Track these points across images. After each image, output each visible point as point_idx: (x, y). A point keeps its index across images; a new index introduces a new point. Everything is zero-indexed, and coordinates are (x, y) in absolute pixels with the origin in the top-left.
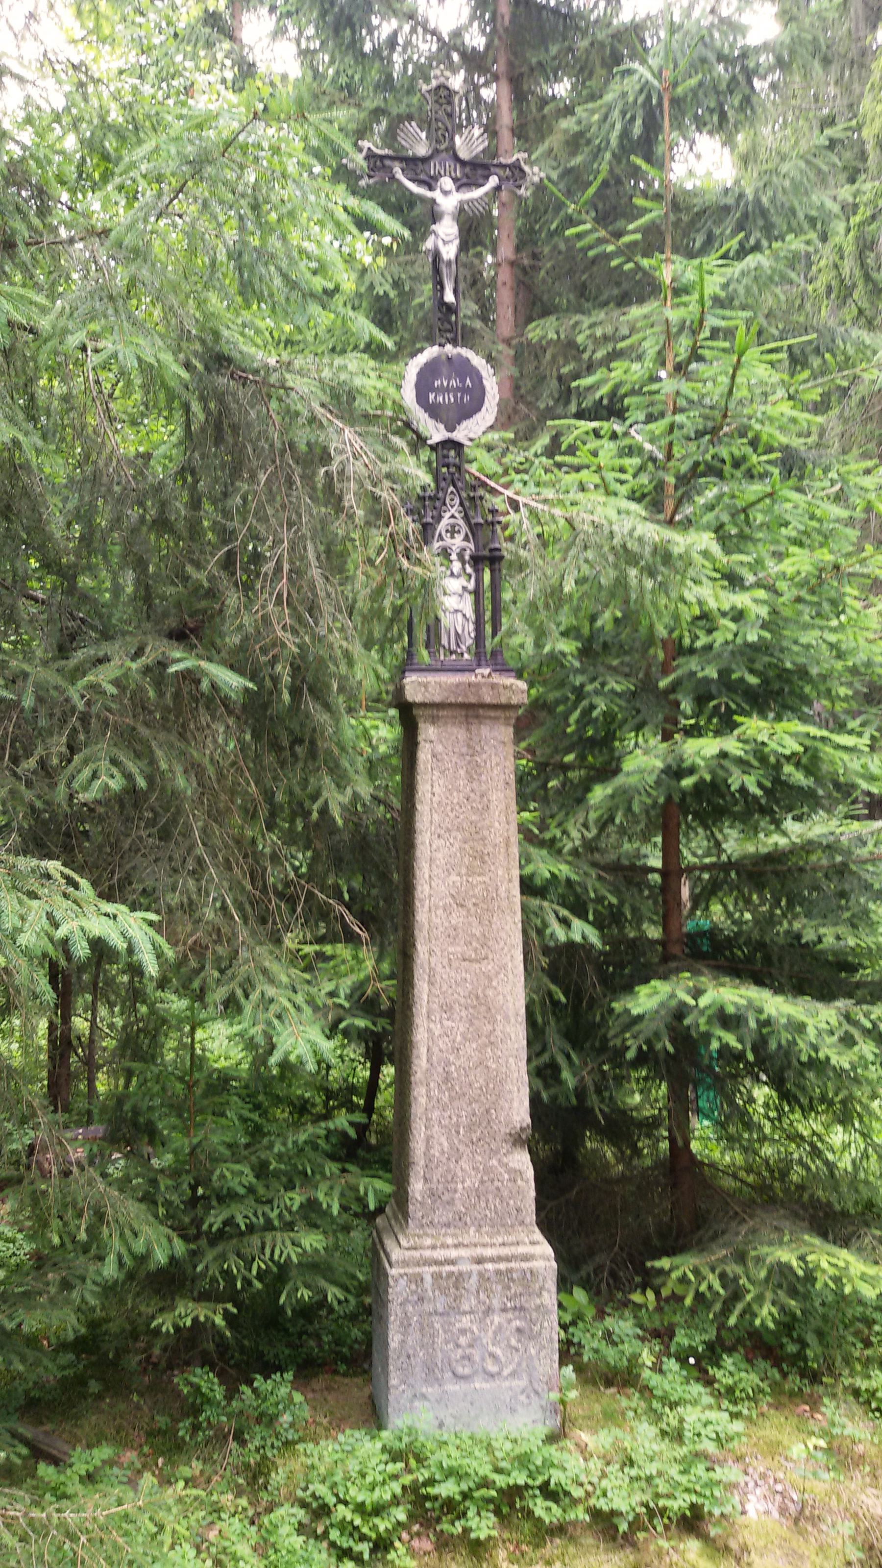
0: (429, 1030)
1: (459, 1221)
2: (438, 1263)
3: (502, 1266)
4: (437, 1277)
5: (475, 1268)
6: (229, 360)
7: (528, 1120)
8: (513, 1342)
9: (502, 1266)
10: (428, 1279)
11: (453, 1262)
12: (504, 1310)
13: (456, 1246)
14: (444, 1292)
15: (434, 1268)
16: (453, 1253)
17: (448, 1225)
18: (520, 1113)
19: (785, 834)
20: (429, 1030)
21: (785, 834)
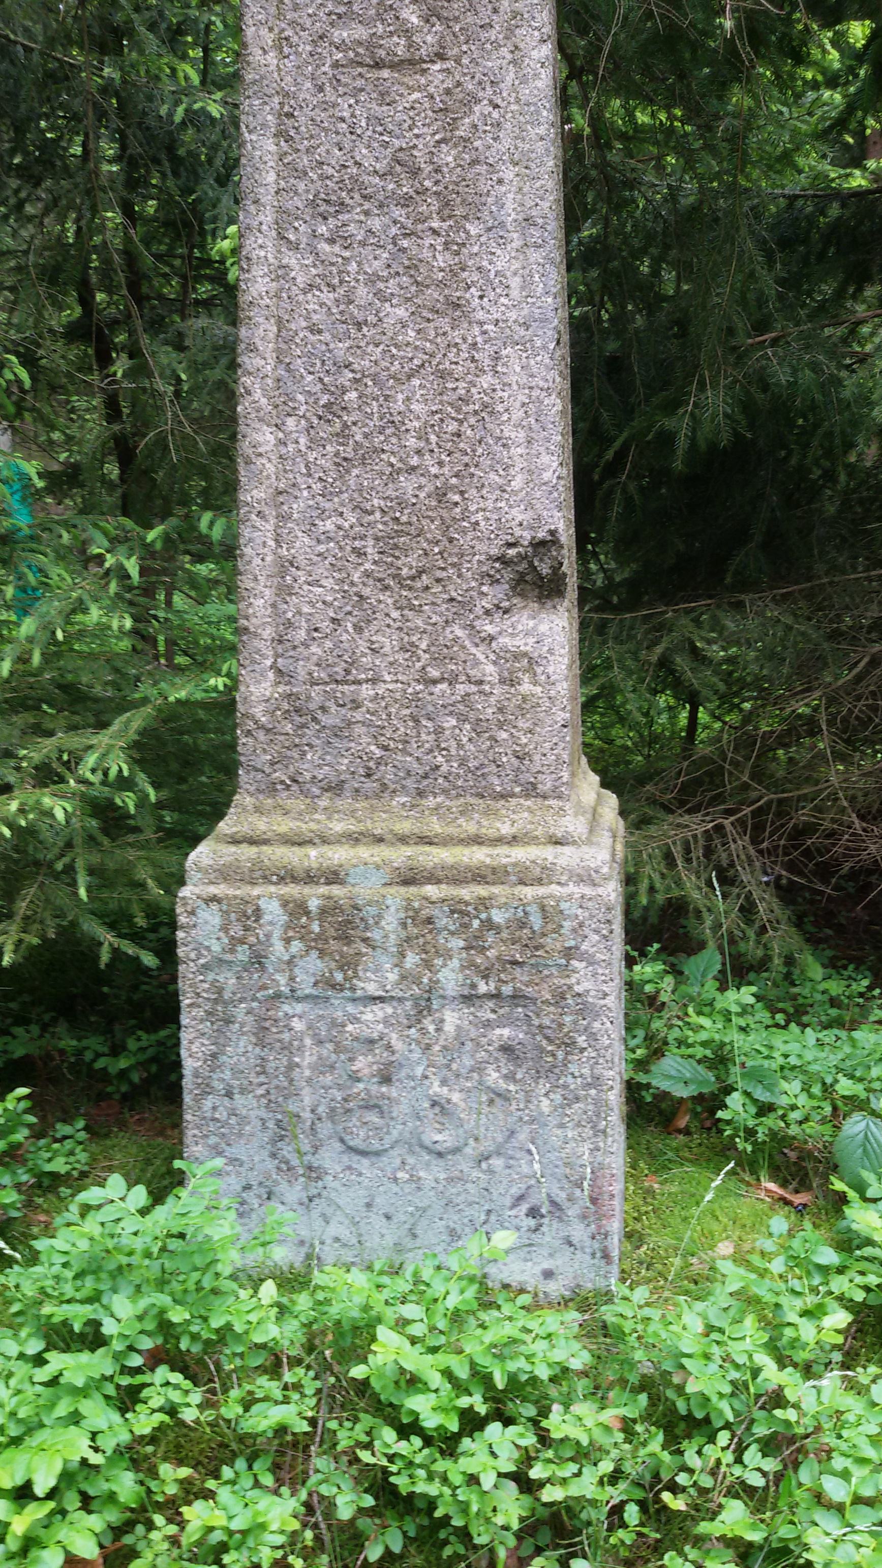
0: (281, 273)
1: (371, 782)
2: (288, 876)
3: (467, 893)
4: (297, 909)
5: (396, 897)
6: (627, 983)
7: (560, 521)
8: (493, 1077)
9: (467, 893)
10: (273, 911)
11: (334, 877)
12: (469, 999)
13: (354, 839)
14: (317, 945)
15: (291, 890)
16: (338, 855)
17: (335, 788)
18: (531, 482)
19: (109, 1420)
20: (281, 273)
21: (109, 1420)
